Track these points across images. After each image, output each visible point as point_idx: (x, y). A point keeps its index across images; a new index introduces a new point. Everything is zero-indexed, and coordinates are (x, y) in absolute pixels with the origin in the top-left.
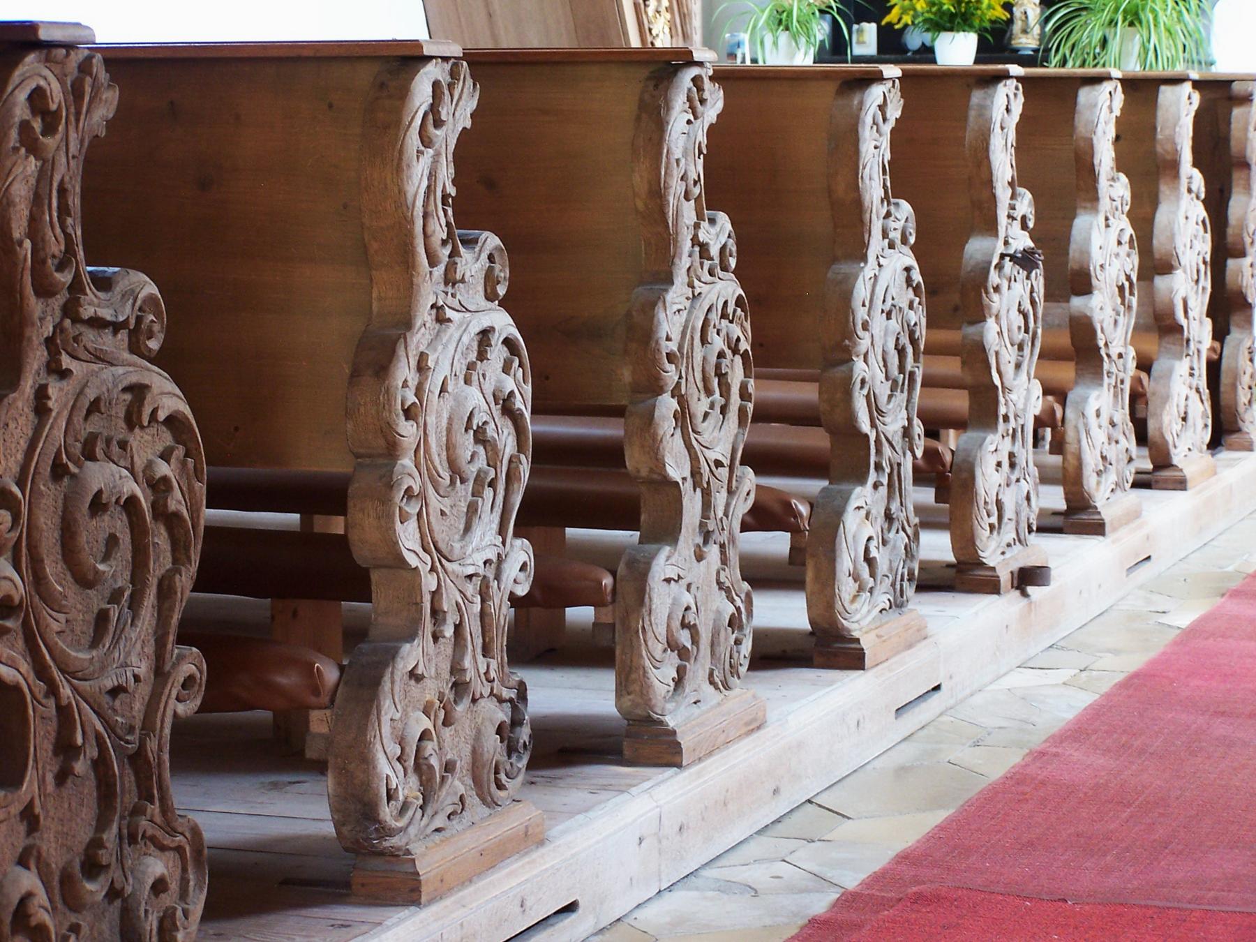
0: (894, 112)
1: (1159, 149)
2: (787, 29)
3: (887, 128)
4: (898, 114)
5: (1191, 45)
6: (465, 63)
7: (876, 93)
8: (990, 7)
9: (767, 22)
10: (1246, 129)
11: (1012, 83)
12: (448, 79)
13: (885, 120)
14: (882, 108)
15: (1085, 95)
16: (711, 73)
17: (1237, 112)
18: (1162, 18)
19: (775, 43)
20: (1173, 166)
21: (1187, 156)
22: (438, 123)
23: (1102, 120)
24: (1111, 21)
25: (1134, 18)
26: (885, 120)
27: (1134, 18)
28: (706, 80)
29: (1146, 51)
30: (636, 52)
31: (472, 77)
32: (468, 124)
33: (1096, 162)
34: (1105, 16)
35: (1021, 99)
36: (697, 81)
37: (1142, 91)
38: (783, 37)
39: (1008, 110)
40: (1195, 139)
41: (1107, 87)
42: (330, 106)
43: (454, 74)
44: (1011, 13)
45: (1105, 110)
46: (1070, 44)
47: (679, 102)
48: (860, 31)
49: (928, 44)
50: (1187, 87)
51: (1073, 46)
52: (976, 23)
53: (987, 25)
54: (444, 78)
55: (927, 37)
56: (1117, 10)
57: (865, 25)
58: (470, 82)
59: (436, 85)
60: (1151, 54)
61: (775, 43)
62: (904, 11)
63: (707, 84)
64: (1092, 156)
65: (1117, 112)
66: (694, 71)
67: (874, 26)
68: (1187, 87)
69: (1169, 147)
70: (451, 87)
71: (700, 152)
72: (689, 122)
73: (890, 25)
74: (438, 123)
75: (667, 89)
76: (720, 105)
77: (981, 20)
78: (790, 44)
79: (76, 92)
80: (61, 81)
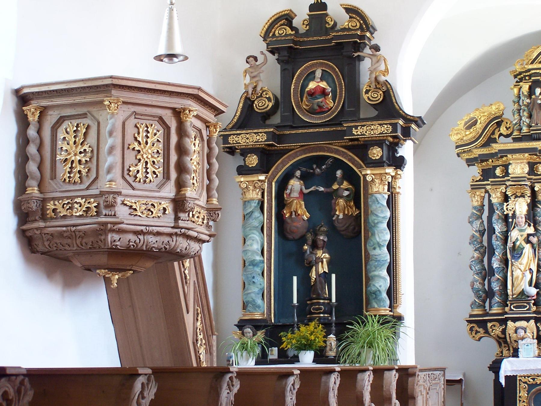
0: (297, 386)
1: (384, 394)
2: (246, 350)
3: (295, 392)
4: (298, 387)
5: (390, 354)
6: (153, 376)
7: (291, 379)
8: (319, 342)
9: (239, 347)
10: (414, 385)
11: (336, 374)
12: (147, 381)
13: (294, 389)
14: (293, 385)
15: (360, 376)
16: (236, 375)
17: (410, 379)
18: (381, 345)
19: (242, 355)
20: (390, 399)
21: (394, 396)
22: (143, 398)
23: (366, 384)
24: (362, 346)
25: (370, 345)
26: (294, 389)
27: (370, 345)
28: (234, 378)
29: (375, 357)
30: (205, 368)
31: (155, 381)
32: (153, 398)
33: (364, 400)
34: (360, 345)
35: (339, 379)
36: (231, 378)
37: (379, 373)
38: (245, 353)
39: (335, 383)
40: (396, 390)
41: (368, 373)
42: (103, 392)
43: (149, 380)
44: (326, 344)
45: (367, 381)
46: (348, 354)
47: (225, 386)
48: (272, 350)
49: (296, 355)
50: (394, 372)
51: (349, 355)
52: (314, 348)
53: (318, 348)
54: (145, 381)
55: (296, 353)
56: (364, 342)
57: (273, 348)
58: (154, 383)
59: (143, 384)
60: (377, 358)
61: (242, 355)
62: (288, 343)
63: (234, 379)
64: (363, 397)
65: (371, 382)
66: (230, 375)
67: (277, 348)
68: (394, 372)
69: (388, 393)
70: (148, 384)
71: (232, 404)
72: (228, 393)
73: (283, 348)
74: (143, 398)
75: (220, 382)
76: (238, 386)
77: (316, 346)
78: (247, 355)
79: (19, 392)
80: (13, 388)
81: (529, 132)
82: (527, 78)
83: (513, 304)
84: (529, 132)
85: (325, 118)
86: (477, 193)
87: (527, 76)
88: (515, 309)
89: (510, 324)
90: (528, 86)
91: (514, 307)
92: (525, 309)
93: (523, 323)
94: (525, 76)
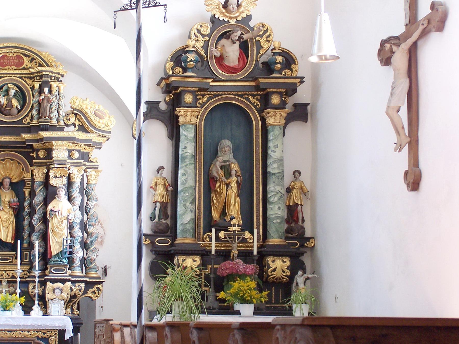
81: (38, 123)
82: (38, 78)
83: (10, 262)
84: (38, 123)
85: (247, 71)
86: (41, 170)
87: (38, 76)
88: (54, 272)
89: (49, 284)
90: (38, 85)
91: (53, 270)
92: (63, 273)
93: (59, 285)
94: (36, 76)
